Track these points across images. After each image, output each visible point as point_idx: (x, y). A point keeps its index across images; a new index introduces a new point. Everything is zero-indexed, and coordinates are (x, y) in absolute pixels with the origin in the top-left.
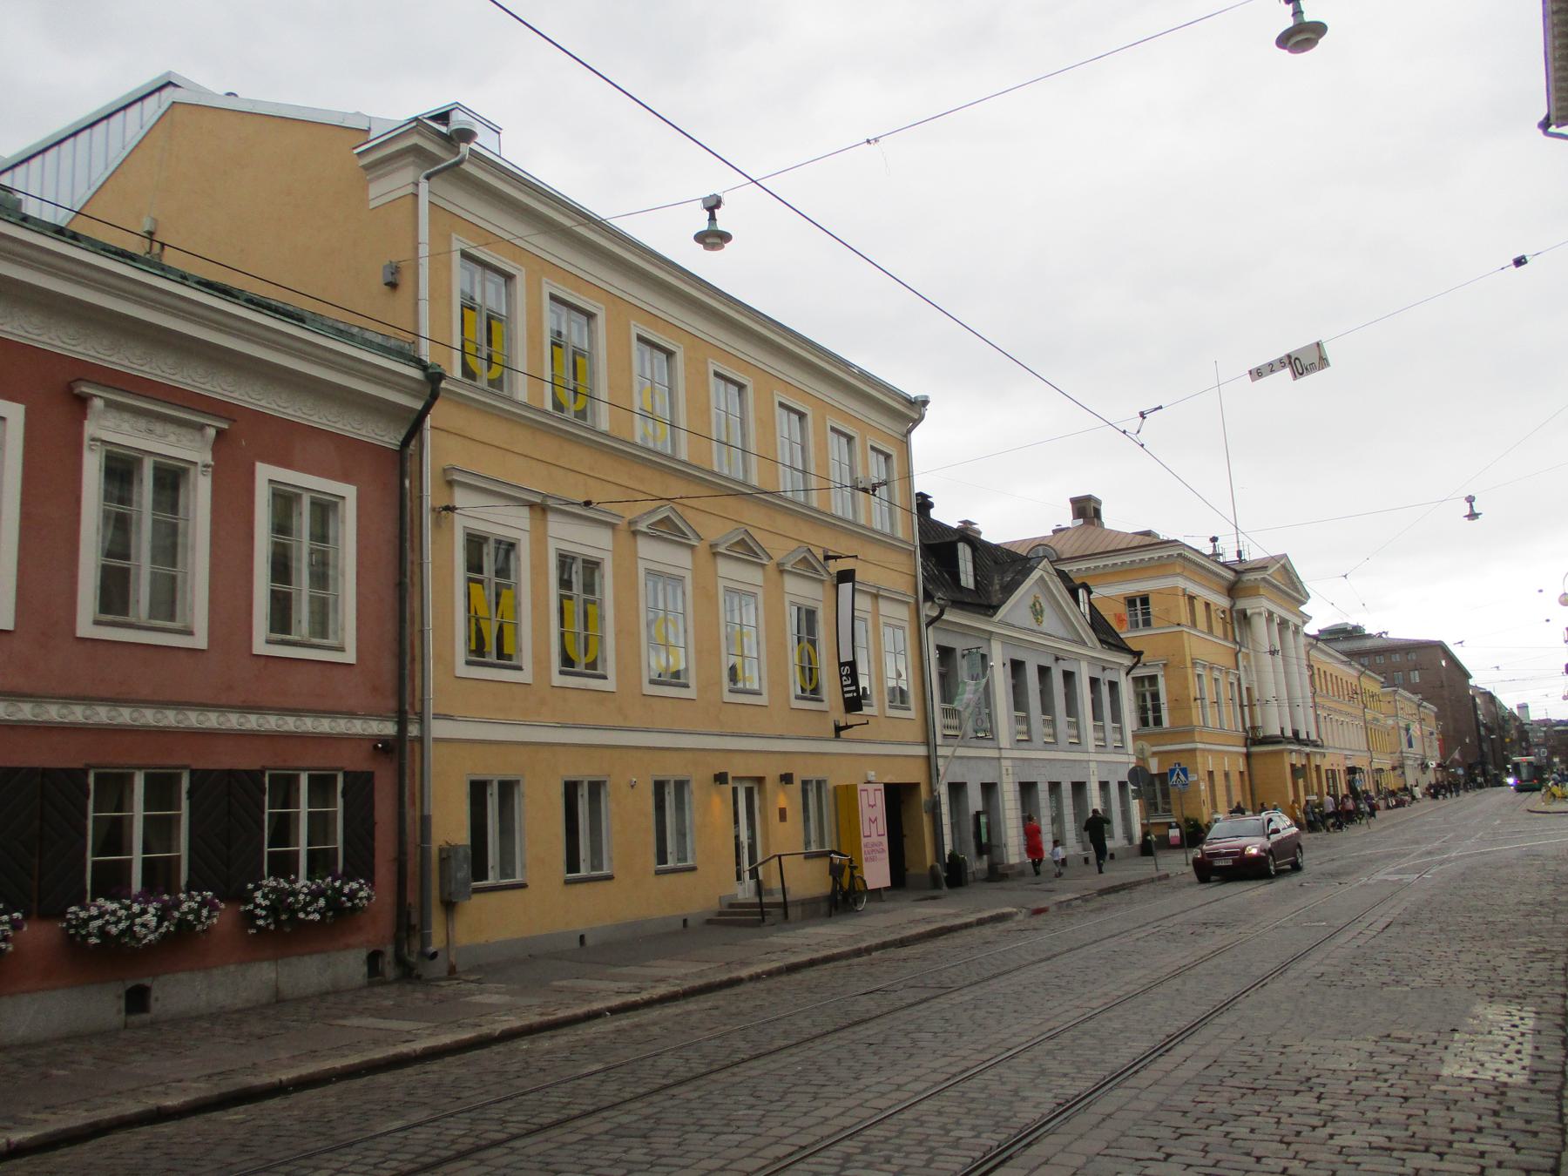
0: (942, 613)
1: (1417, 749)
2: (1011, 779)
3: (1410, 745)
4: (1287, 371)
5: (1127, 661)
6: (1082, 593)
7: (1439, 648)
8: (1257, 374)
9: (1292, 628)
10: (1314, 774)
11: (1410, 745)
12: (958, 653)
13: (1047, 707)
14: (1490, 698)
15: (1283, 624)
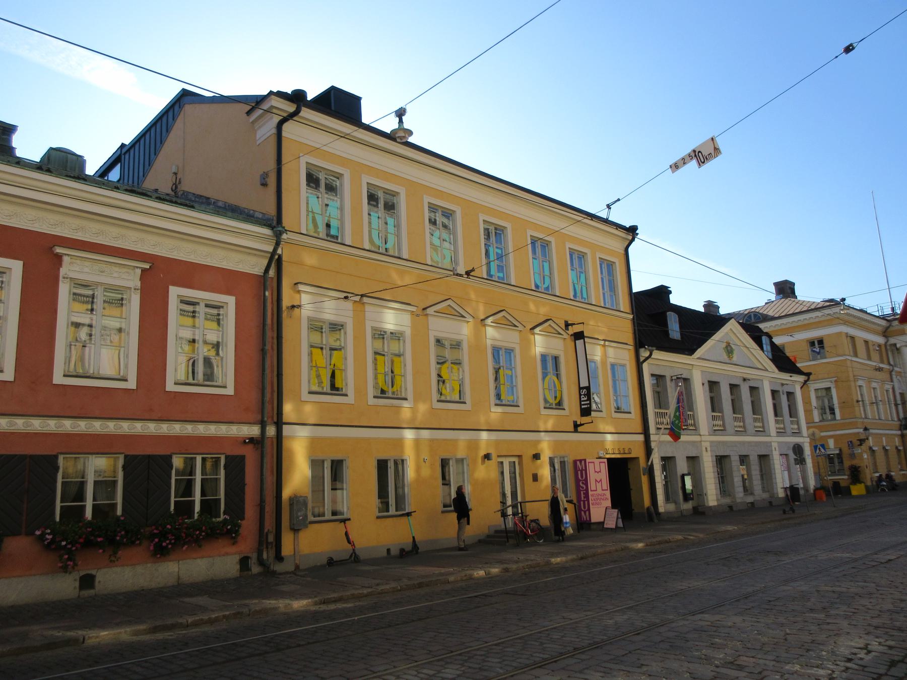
0: (651, 354)
2: (709, 453)
4: (694, 162)
6: (764, 339)
8: (675, 167)
10: (645, 479)
12: (668, 379)
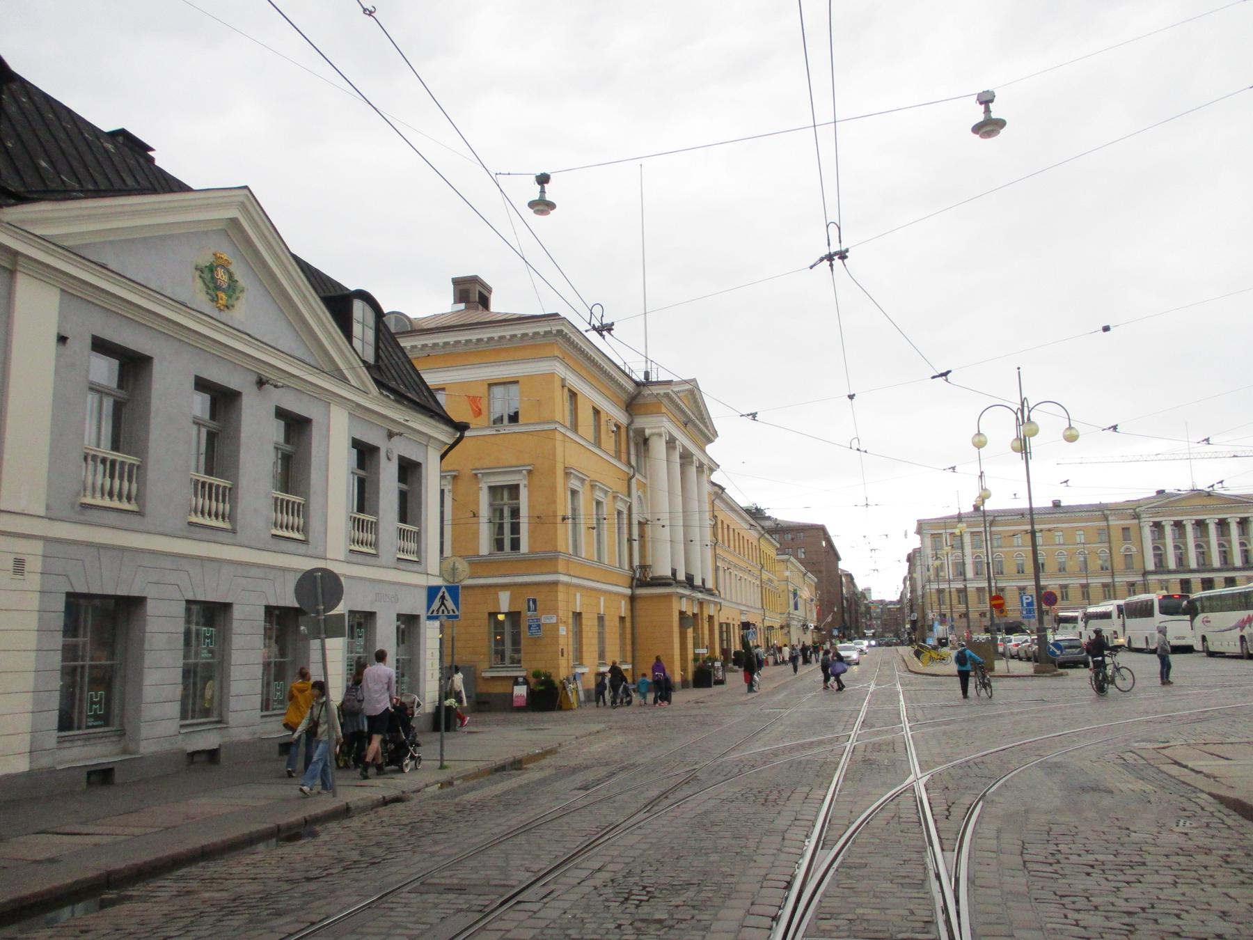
1: (800, 612)
3: (796, 608)
5: (444, 434)
7: (821, 531)
9: (696, 463)
10: (706, 626)
11: (796, 608)
14: (850, 577)
15: (686, 457)
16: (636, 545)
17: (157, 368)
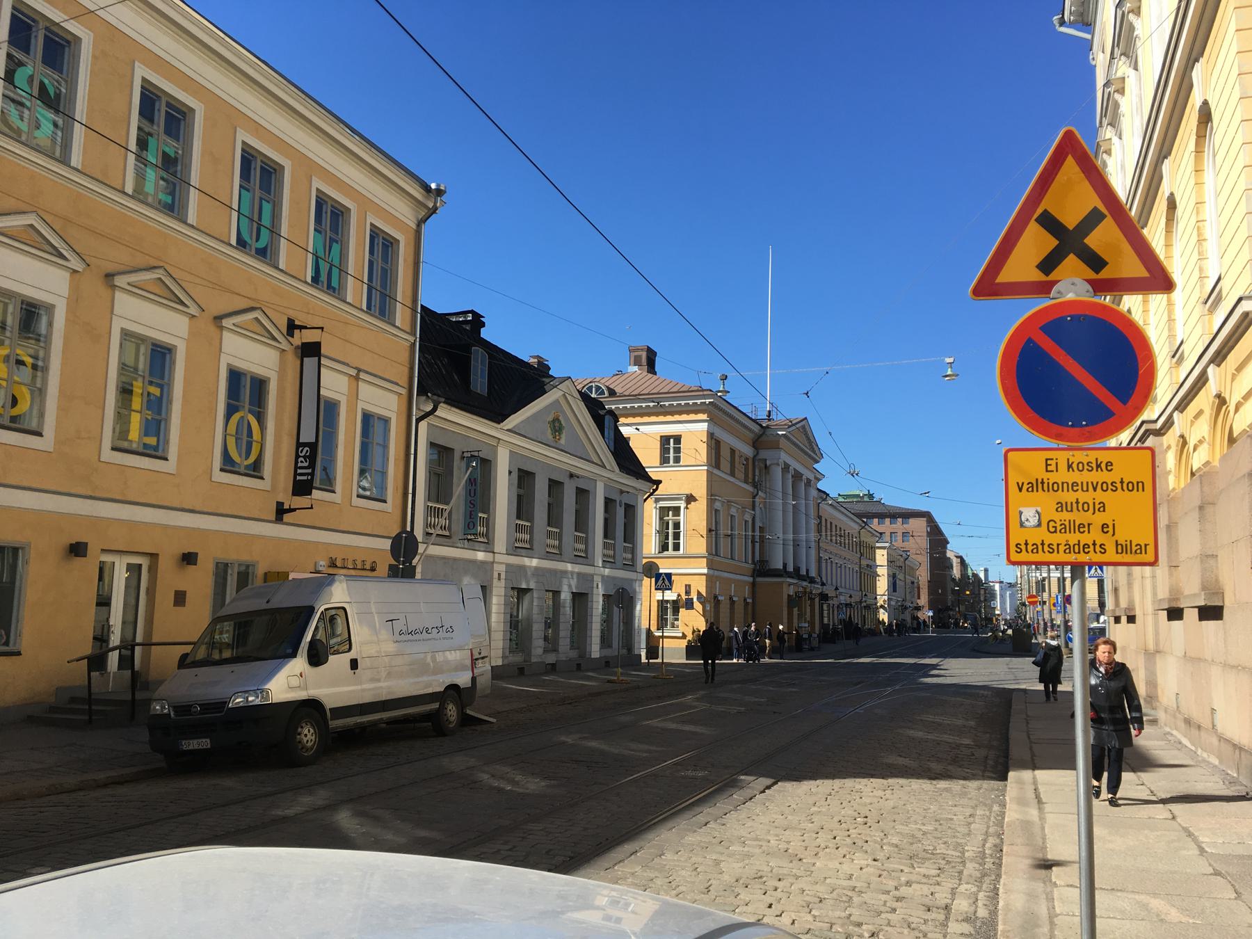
0: (435, 409)
12: (457, 456)
13: (554, 517)
15: (797, 476)
16: (757, 545)
17: (566, 486)
